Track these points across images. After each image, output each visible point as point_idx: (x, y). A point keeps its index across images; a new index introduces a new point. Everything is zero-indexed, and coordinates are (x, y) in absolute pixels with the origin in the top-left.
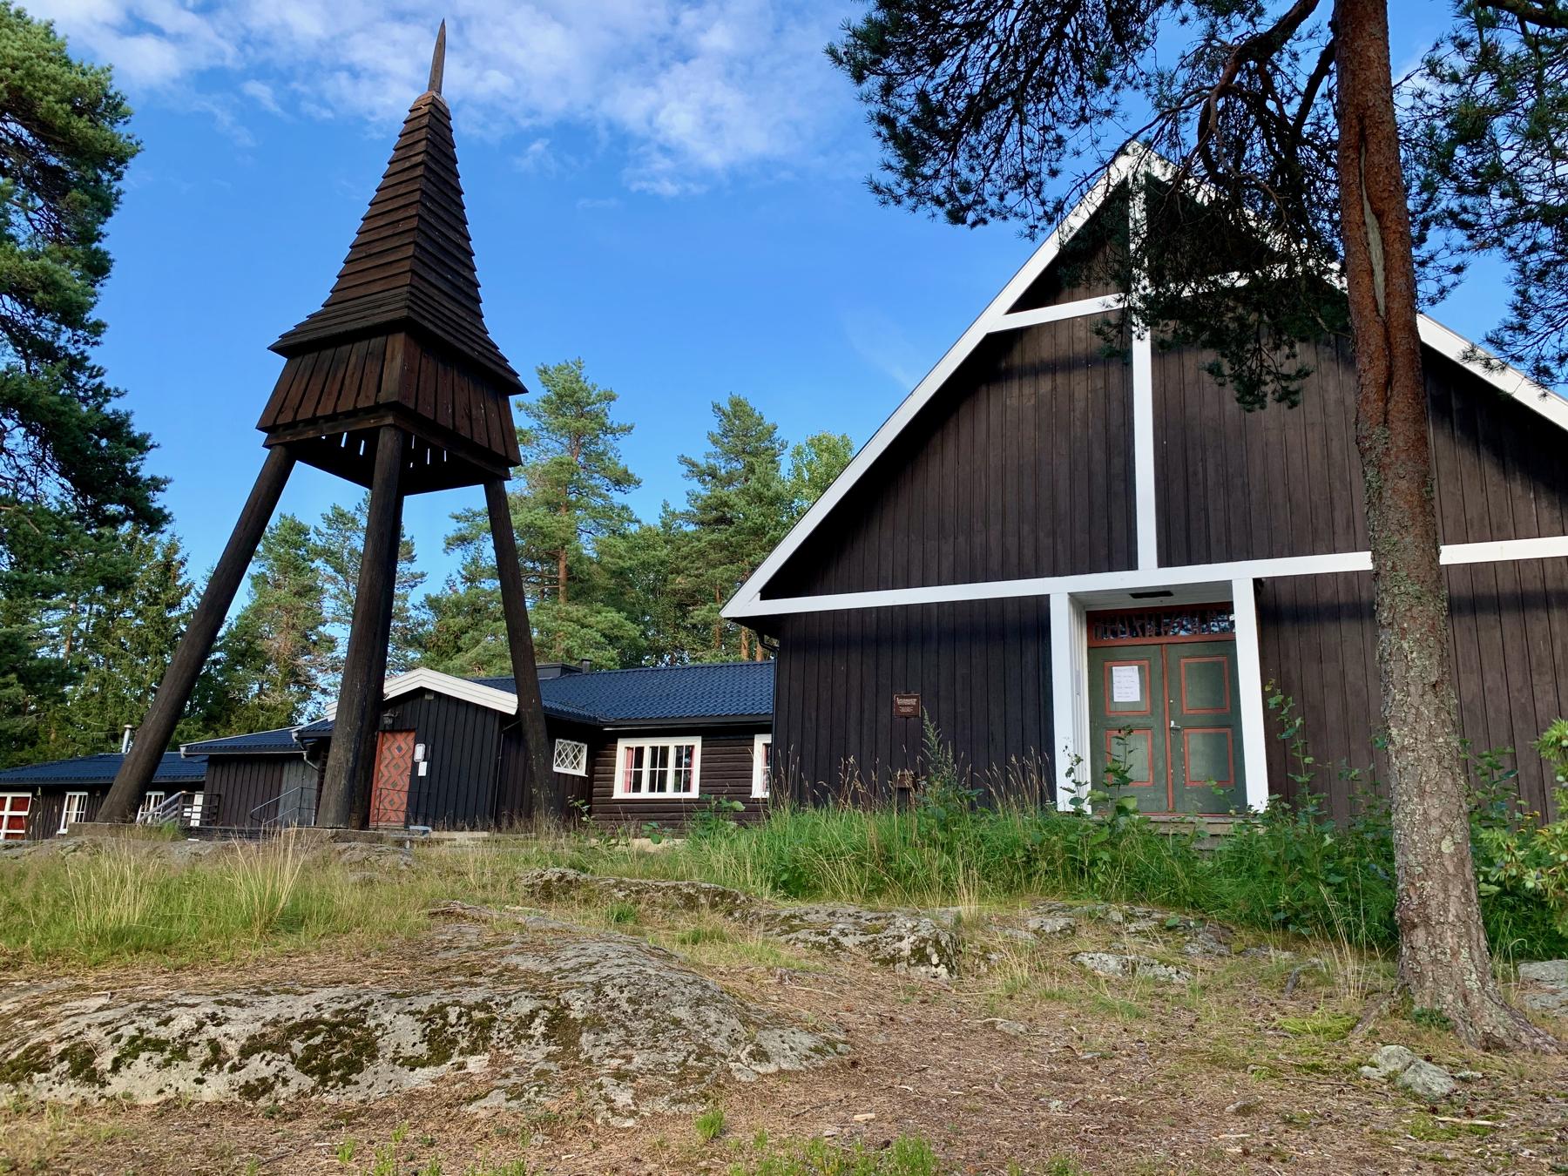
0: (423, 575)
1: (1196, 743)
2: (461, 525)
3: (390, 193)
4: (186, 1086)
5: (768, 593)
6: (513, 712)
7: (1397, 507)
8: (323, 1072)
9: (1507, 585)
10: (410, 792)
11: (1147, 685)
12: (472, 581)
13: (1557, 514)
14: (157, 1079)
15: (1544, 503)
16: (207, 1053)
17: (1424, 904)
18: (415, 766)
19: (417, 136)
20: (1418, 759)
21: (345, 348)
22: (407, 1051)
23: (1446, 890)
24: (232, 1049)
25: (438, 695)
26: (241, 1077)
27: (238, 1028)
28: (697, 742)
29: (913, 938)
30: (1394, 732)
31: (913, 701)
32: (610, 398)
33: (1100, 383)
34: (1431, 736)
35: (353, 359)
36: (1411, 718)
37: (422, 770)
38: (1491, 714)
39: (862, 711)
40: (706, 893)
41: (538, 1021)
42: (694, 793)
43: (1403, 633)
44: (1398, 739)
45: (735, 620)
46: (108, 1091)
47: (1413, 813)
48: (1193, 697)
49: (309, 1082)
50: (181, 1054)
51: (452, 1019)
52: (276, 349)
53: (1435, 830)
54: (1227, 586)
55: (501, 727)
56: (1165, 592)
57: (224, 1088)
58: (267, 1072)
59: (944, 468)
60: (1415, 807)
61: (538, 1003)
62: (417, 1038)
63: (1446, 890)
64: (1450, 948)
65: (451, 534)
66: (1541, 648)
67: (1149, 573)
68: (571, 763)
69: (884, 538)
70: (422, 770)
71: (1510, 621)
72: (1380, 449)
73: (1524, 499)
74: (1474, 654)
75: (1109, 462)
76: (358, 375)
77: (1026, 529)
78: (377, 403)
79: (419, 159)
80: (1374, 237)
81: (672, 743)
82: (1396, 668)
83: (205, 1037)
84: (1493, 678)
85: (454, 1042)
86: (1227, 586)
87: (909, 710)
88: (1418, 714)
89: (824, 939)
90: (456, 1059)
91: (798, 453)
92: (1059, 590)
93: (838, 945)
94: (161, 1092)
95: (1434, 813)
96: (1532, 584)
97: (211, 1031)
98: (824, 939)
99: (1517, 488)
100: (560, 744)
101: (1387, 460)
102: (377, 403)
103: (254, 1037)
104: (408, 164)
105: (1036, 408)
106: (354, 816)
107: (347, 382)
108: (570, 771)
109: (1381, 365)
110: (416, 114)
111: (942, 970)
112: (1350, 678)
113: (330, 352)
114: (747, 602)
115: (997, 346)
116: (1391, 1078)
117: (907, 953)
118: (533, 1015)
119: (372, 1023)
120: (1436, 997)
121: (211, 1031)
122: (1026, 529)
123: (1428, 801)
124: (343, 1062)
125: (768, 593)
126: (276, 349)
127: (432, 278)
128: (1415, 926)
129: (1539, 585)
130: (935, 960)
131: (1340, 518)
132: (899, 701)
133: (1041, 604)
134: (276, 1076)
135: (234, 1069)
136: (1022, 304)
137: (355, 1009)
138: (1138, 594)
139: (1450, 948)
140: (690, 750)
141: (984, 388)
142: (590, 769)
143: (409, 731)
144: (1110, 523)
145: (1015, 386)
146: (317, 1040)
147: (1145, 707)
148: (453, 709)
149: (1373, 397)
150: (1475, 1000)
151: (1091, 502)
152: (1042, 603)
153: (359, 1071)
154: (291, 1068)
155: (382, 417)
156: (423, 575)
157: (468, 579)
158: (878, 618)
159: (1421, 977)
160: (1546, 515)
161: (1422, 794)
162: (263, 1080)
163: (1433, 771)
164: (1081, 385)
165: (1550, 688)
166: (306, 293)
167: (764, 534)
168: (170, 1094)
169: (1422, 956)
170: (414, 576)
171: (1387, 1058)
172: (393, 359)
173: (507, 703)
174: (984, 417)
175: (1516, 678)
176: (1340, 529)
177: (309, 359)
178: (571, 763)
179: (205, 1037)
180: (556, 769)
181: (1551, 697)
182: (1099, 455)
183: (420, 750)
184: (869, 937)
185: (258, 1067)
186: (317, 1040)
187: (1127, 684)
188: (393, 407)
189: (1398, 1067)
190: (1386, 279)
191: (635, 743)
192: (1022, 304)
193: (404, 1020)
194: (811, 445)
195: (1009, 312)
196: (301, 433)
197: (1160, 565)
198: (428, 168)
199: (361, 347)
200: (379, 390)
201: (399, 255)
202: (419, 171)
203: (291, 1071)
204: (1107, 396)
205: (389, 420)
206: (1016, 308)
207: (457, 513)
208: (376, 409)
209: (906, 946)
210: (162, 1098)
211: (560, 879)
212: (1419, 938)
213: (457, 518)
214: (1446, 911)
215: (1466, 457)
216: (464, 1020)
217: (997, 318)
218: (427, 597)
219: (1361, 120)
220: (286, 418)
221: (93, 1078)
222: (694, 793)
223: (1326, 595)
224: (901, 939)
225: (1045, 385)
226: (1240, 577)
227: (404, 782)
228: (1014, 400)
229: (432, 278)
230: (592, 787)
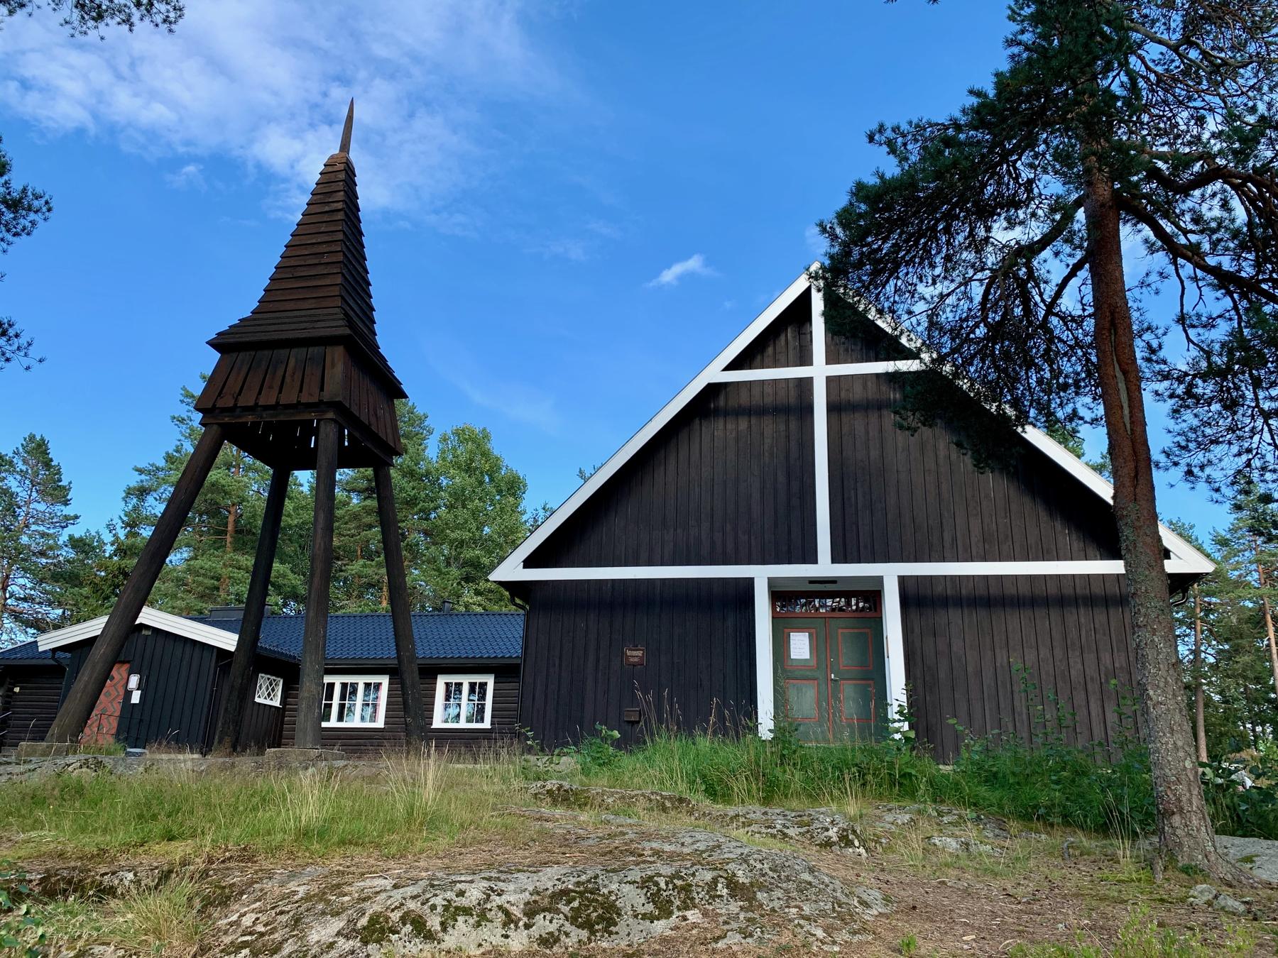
0: (77, 517)
1: (848, 690)
2: (143, 477)
3: (312, 229)
4: (497, 940)
5: (530, 563)
6: (232, 649)
7: (1146, 554)
8: (588, 925)
9: (1052, 590)
10: (121, 717)
11: (814, 647)
12: (132, 527)
13: (1082, 545)
14: (475, 936)
15: (1074, 536)
16: (501, 916)
17: (1179, 800)
18: (128, 694)
19: (334, 187)
20: (1168, 710)
21: (283, 352)
22: (641, 910)
23: (1190, 791)
24: (516, 912)
25: (156, 631)
26: (535, 931)
27: (514, 896)
28: (385, 681)
29: (835, 829)
30: (1151, 693)
31: (640, 653)
32: (1192, 527)
33: (782, 427)
34: (1175, 696)
35: (292, 362)
36: (1162, 685)
37: (136, 698)
38: (1043, 676)
39: (598, 661)
40: (670, 798)
41: (720, 886)
42: (487, 724)
43: (1154, 632)
44: (1154, 698)
45: (501, 583)
46: (443, 946)
47: (1167, 743)
48: (846, 657)
49: (584, 934)
50: (483, 918)
51: (663, 885)
52: (212, 344)
53: (1181, 754)
54: (879, 580)
55: (217, 662)
56: (832, 581)
57: (525, 941)
58: (552, 928)
59: (666, 475)
60: (1168, 740)
61: (715, 873)
62: (643, 900)
63: (1190, 791)
64: (1193, 827)
65: (133, 484)
66: (1073, 633)
67: (825, 567)
68: (269, 694)
69: (617, 525)
70: (136, 698)
71: (1055, 614)
72: (1134, 517)
73: (1065, 536)
74: (1033, 636)
75: (789, 484)
76: (299, 375)
77: (729, 527)
78: (299, 402)
79: (340, 206)
80: (1122, 386)
81: (361, 680)
82: (1150, 654)
83: (494, 904)
84: (1044, 652)
85: (670, 902)
86: (879, 580)
87: (636, 660)
88: (1166, 683)
89: (774, 831)
90: (677, 913)
91: (444, 439)
92: (761, 575)
93: (785, 835)
94: (480, 945)
95: (1180, 743)
96: (1097, 589)
97: (497, 900)
98: (774, 831)
99: (1058, 525)
100: (263, 680)
101: (1137, 524)
102: (299, 402)
103: (528, 903)
104: (327, 209)
105: (737, 440)
106: (227, 739)
107: (288, 379)
108: (268, 702)
109: (1132, 465)
110: (330, 169)
111: (862, 850)
112: (954, 648)
113: (267, 353)
114: (512, 569)
115: (712, 390)
116: (1209, 903)
117: (835, 839)
118: (715, 881)
119: (605, 891)
120: (1191, 858)
121: (497, 900)
122: (729, 527)
123: (1177, 736)
124: (601, 918)
125: (530, 563)
126: (212, 344)
127: (351, 302)
128: (1173, 813)
129: (1072, 591)
130: (857, 843)
131: (947, 537)
132: (629, 653)
133: (747, 586)
134: (559, 931)
135: (527, 927)
136: (732, 366)
137: (589, 881)
138: (813, 581)
139: (1193, 827)
140: (483, 686)
141: (697, 421)
142: (283, 701)
143: (123, 662)
144: (789, 527)
145: (720, 423)
146: (576, 904)
147: (813, 663)
148: (188, 648)
149: (1128, 484)
150: (1213, 858)
151: (776, 513)
152: (749, 583)
153: (615, 924)
154: (567, 924)
155: (324, 412)
156: (77, 517)
157: (127, 525)
158: (613, 587)
159: (1180, 845)
160: (1075, 545)
161: (1172, 731)
162: (551, 934)
163: (1177, 717)
164: (770, 428)
165: (1079, 660)
166: (239, 300)
167: (416, 505)
168: (487, 947)
169: (1178, 832)
170: (67, 518)
171: (1201, 892)
172: (333, 366)
173: (227, 640)
174: (697, 440)
175: (1058, 652)
176: (947, 545)
177: (244, 356)
178: (269, 694)
179: (494, 904)
180: (257, 700)
181: (1080, 666)
182: (781, 478)
183: (134, 680)
184: (805, 829)
185: (544, 924)
186: (576, 904)
187: (800, 646)
188: (337, 406)
189: (1210, 897)
190: (1130, 412)
191: (454, 679)
192: (732, 366)
193: (626, 888)
194: (456, 433)
195: (726, 369)
196: (239, 417)
197: (816, 562)
198: (346, 214)
199: (296, 354)
200: (322, 389)
201: (328, 282)
202: (340, 216)
203: (568, 927)
204: (788, 437)
205: (330, 415)
206: (729, 367)
207: (140, 466)
208: (319, 406)
209: (833, 833)
210: (482, 950)
211: (559, 789)
212: (1176, 820)
213: (141, 471)
214: (1191, 803)
215: (1027, 500)
216: (671, 886)
217: (715, 373)
218: (71, 537)
219: (1112, 313)
220: (227, 402)
221: (430, 936)
222: (487, 724)
223: (939, 589)
224: (827, 830)
225: (743, 424)
226: (890, 574)
227: (116, 709)
228: (718, 432)
229: (351, 302)
230: (284, 716)
